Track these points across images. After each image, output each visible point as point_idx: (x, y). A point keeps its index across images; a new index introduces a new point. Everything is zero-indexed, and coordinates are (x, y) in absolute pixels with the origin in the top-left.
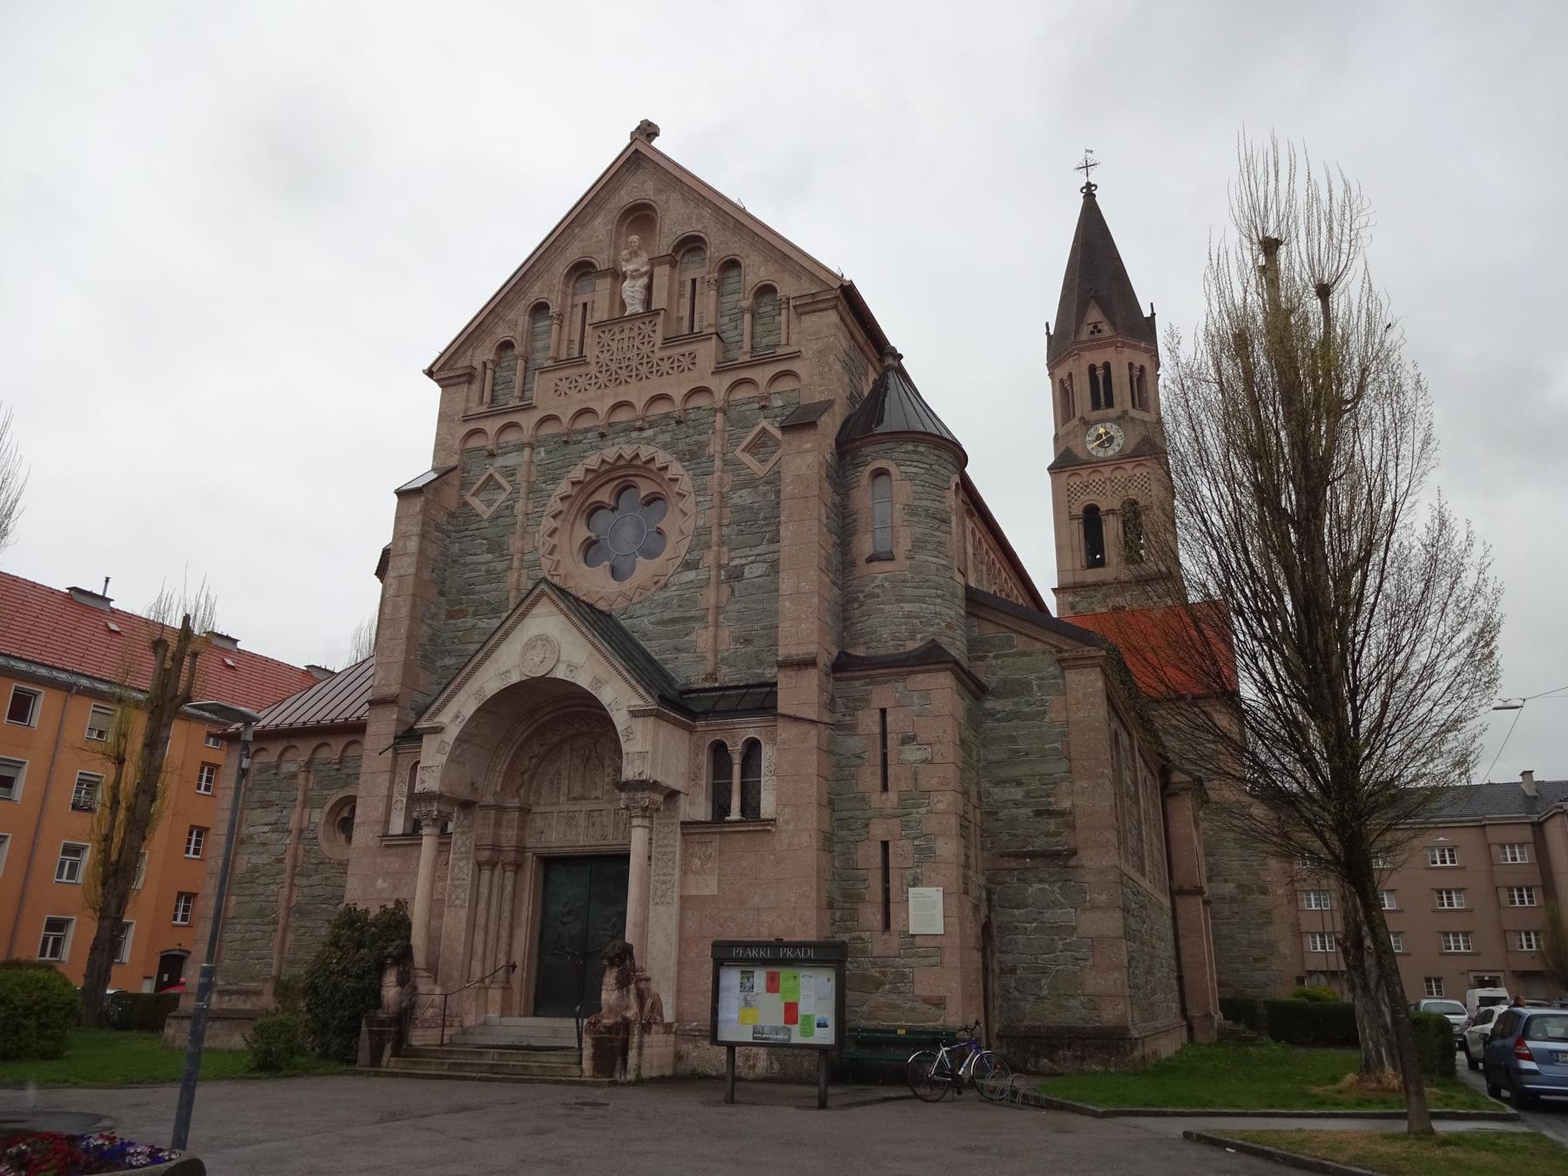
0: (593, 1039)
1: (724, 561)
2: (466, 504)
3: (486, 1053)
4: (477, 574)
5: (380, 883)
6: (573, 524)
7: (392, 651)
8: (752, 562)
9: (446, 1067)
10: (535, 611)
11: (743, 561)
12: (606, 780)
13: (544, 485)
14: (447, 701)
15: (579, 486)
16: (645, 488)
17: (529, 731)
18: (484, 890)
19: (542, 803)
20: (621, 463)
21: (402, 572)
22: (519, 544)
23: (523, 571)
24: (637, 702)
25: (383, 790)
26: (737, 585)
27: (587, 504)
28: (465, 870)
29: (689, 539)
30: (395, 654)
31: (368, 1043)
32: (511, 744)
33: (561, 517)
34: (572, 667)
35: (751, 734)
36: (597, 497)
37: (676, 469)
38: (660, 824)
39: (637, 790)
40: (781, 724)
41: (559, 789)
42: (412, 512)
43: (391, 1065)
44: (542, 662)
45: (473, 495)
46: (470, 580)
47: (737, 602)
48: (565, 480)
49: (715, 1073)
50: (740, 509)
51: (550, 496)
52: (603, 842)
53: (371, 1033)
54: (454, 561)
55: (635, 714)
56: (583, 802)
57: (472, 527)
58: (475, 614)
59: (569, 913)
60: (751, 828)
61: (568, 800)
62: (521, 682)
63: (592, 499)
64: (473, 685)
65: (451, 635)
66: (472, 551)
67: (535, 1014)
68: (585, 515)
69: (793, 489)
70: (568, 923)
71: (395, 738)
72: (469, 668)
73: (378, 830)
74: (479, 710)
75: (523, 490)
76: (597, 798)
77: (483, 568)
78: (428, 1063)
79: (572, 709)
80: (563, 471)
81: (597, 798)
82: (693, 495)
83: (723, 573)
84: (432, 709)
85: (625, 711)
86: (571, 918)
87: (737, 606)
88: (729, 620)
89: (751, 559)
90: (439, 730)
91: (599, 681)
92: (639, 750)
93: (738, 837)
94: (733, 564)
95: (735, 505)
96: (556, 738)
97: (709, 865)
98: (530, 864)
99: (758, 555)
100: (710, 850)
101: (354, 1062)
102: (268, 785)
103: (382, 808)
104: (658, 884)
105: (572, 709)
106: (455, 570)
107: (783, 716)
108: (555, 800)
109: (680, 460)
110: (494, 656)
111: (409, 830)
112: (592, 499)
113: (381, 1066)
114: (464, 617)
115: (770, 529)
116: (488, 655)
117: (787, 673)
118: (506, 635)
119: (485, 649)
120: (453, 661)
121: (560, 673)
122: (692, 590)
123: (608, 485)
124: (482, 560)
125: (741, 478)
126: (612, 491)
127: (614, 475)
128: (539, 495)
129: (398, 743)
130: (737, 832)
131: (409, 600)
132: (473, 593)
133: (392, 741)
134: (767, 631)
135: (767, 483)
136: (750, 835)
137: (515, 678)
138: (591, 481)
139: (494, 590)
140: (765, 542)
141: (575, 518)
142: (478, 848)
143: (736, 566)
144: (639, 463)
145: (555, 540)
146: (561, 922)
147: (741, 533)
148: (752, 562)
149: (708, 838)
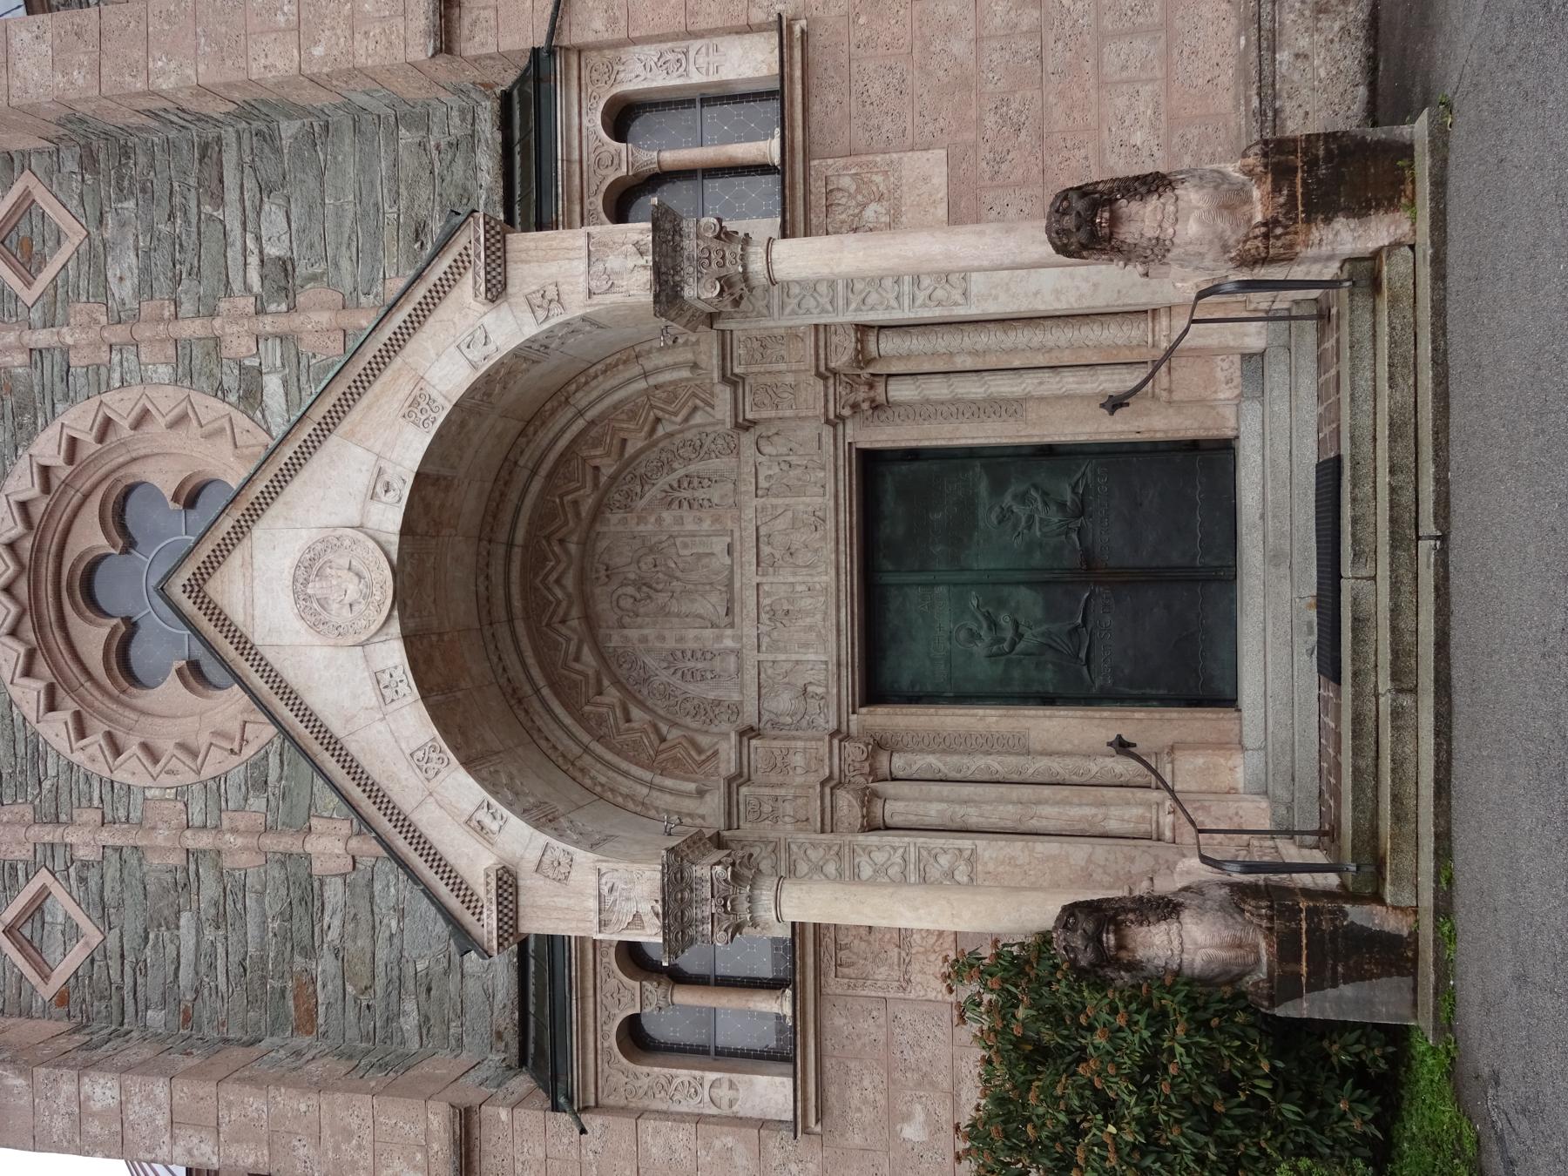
0: (1308, 221)
1: (248, 304)
2: (63, 998)
3: (1355, 602)
4: (220, 950)
5: (913, 1132)
6: (143, 712)
7: (348, 1134)
8: (258, 238)
9: (1406, 701)
10: (237, 615)
11: (254, 260)
12: (690, 526)
13: (47, 785)
14: (437, 860)
15: (60, 693)
16: (90, 537)
17: (559, 710)
18: (933, 812)
19: (736, 697)
20: (22, 588)
21: (162, 1120)
22: (161, 837)
23: (226, 824)
24: (468, 291)
25: (681, 1136)
26: (302, 270)
27: (107, 683)
28: (880, 857)
29: (196, 397)
30: (354, 1123)
31: (1347, 990)
32: (587, 760)
33: (120, 735)
34: (378, 487)
35: (594, 121)
36: (94, 658)
37: (47, 447)
38: (783, 306)
39: (677, 249)
40: (574, 35)
41: (705, 654)
42: (25, 1101)
43: (1407, 899)
44: (359, 576)
45: (45, 978)
46: (235, 970)
47: (336, 265)
48: (40, 728)
49: (1362, 91)
50: (145, 287)
51: (70, 766)
52: (830, 524)
53: (1318, 982)
54: (187, 1019)
55: (496, 289)
56: (737, 585)
57: (114, 974)
58: (309, 952)
59: (994, 625)
60: (798, 73)
61: (732, 625)
62: (409, 640)
63: (98, 668)
64: (404, 785)
65: (351, 1015)
66: (171, 969)
67: (1229, 701)
68: (134, 690)
69: (81, 66)
70: (1016, 625)
71: (555, 1108)
72: (356, 793)
73: (775, 1144)
74: (468, 764)
75: (49, 834)
76: (730, 550)
77: (209, 934)
78: (1397, 764)
79: (515, 590)
80: (20, 736)
81: (730, 551)
82: (106, 398)
83: (273, 307)
84: (453, 903)
85: (490, 320)
86: (1004, 620)
87: (345, 264)
88: (372, 282)
89: (251, 245)
90: (507, 883)
91: (415, 403)
92: (582, 266)
93: (816, 108)
94: (257, 288)
95: (138, 292)
96: (587, 655)
97: (878, 179)
98: (883, 718)
99: (244, 224)
100: (846, 182)
101: (1397, 1036)
102: (184, 375)
103: (727, 1139)
104: (921, 296)
105: (515, 590)
106: (206, 1014)
107: (553, 31)
108: (732, 658)
109: (30, 439)
110: (337, 727)
111: (789, 1068)
112: (98, 668)
113: (1414, 935)
114: (314, 982)
115: (193, 204)
116: (333, 744)
117: (465, 32)
118: (288, 694)
119: (315, 748)
120: (410, 1005)
121: (389, 518)
122: (303, 379)
123: (73, 633)
124: (192, 942)
125: (83, 283)
126: (85, 619)
127: (50, 614)
128: (64, 797)
129: (570, 1100)
130: (805, 109)
131: (231, 1092)
132: (263, 960)
133: (565, 1118)
134: (403, 190)
135: (101, 221)
136: (813, 81)
137: (393, 654)
138: (54, 666)
139: (260, 902)
140: (218, 214)
141: (134, 709)
142: (828, 825)
143: (263, 278)
144: (27, 544)
145: (167, 746)
146: (1013, 645)
147: (196, 273)
148: (258, 238)
149: (818, 187)
